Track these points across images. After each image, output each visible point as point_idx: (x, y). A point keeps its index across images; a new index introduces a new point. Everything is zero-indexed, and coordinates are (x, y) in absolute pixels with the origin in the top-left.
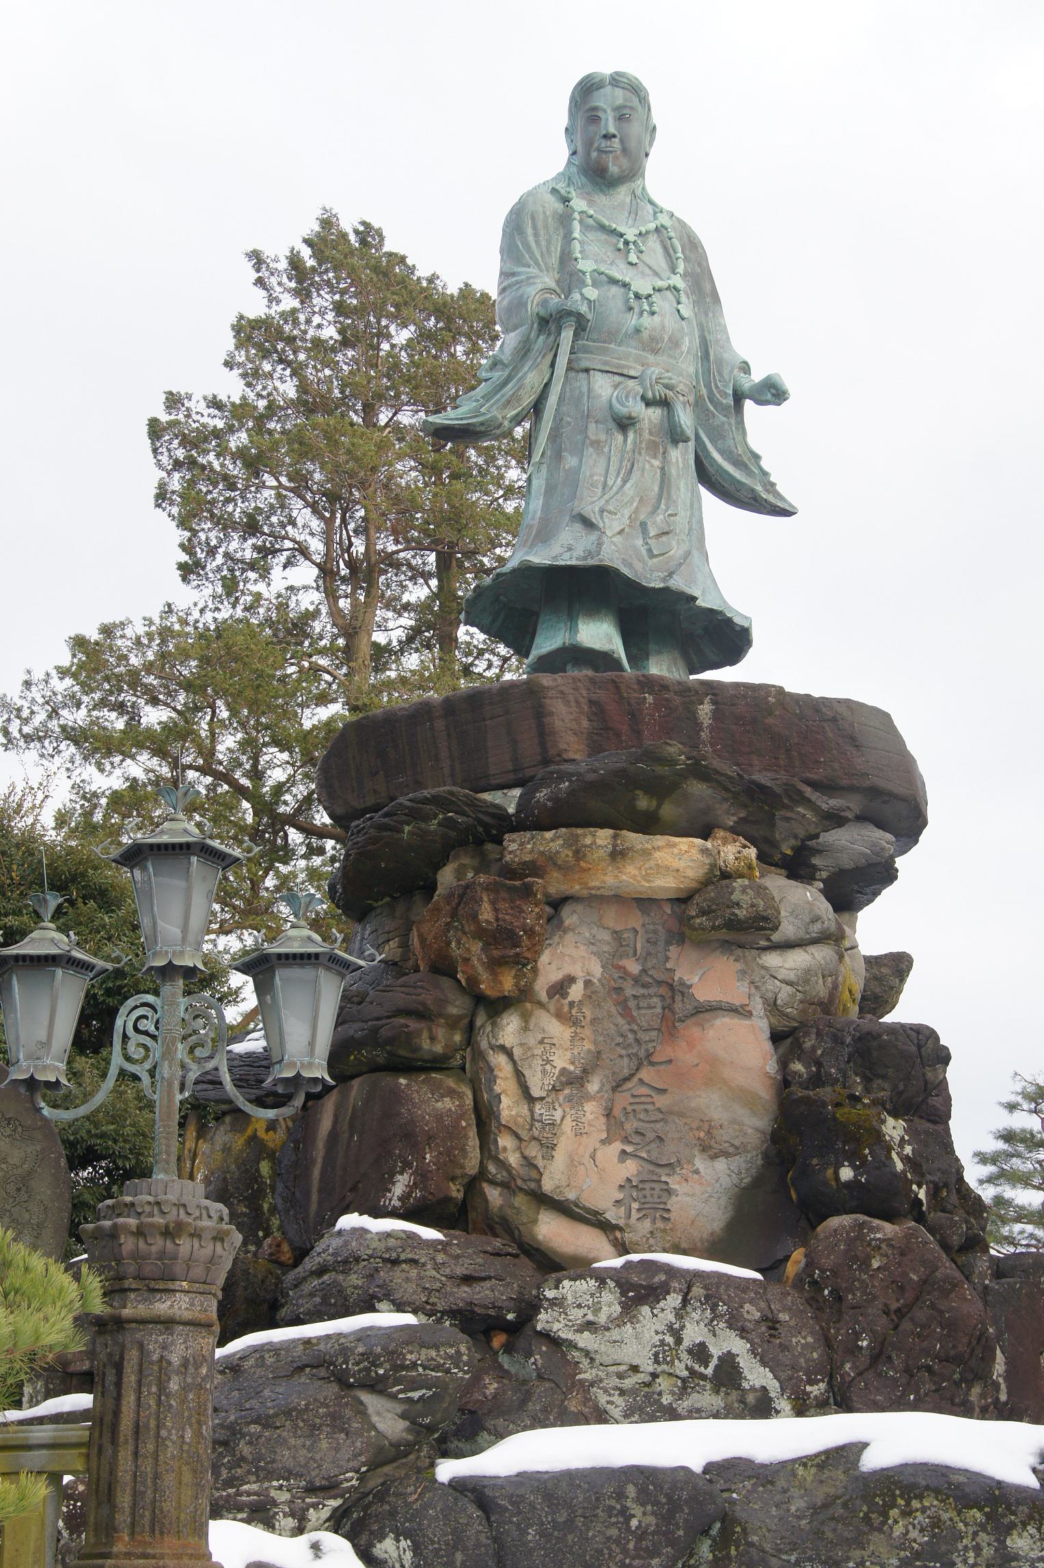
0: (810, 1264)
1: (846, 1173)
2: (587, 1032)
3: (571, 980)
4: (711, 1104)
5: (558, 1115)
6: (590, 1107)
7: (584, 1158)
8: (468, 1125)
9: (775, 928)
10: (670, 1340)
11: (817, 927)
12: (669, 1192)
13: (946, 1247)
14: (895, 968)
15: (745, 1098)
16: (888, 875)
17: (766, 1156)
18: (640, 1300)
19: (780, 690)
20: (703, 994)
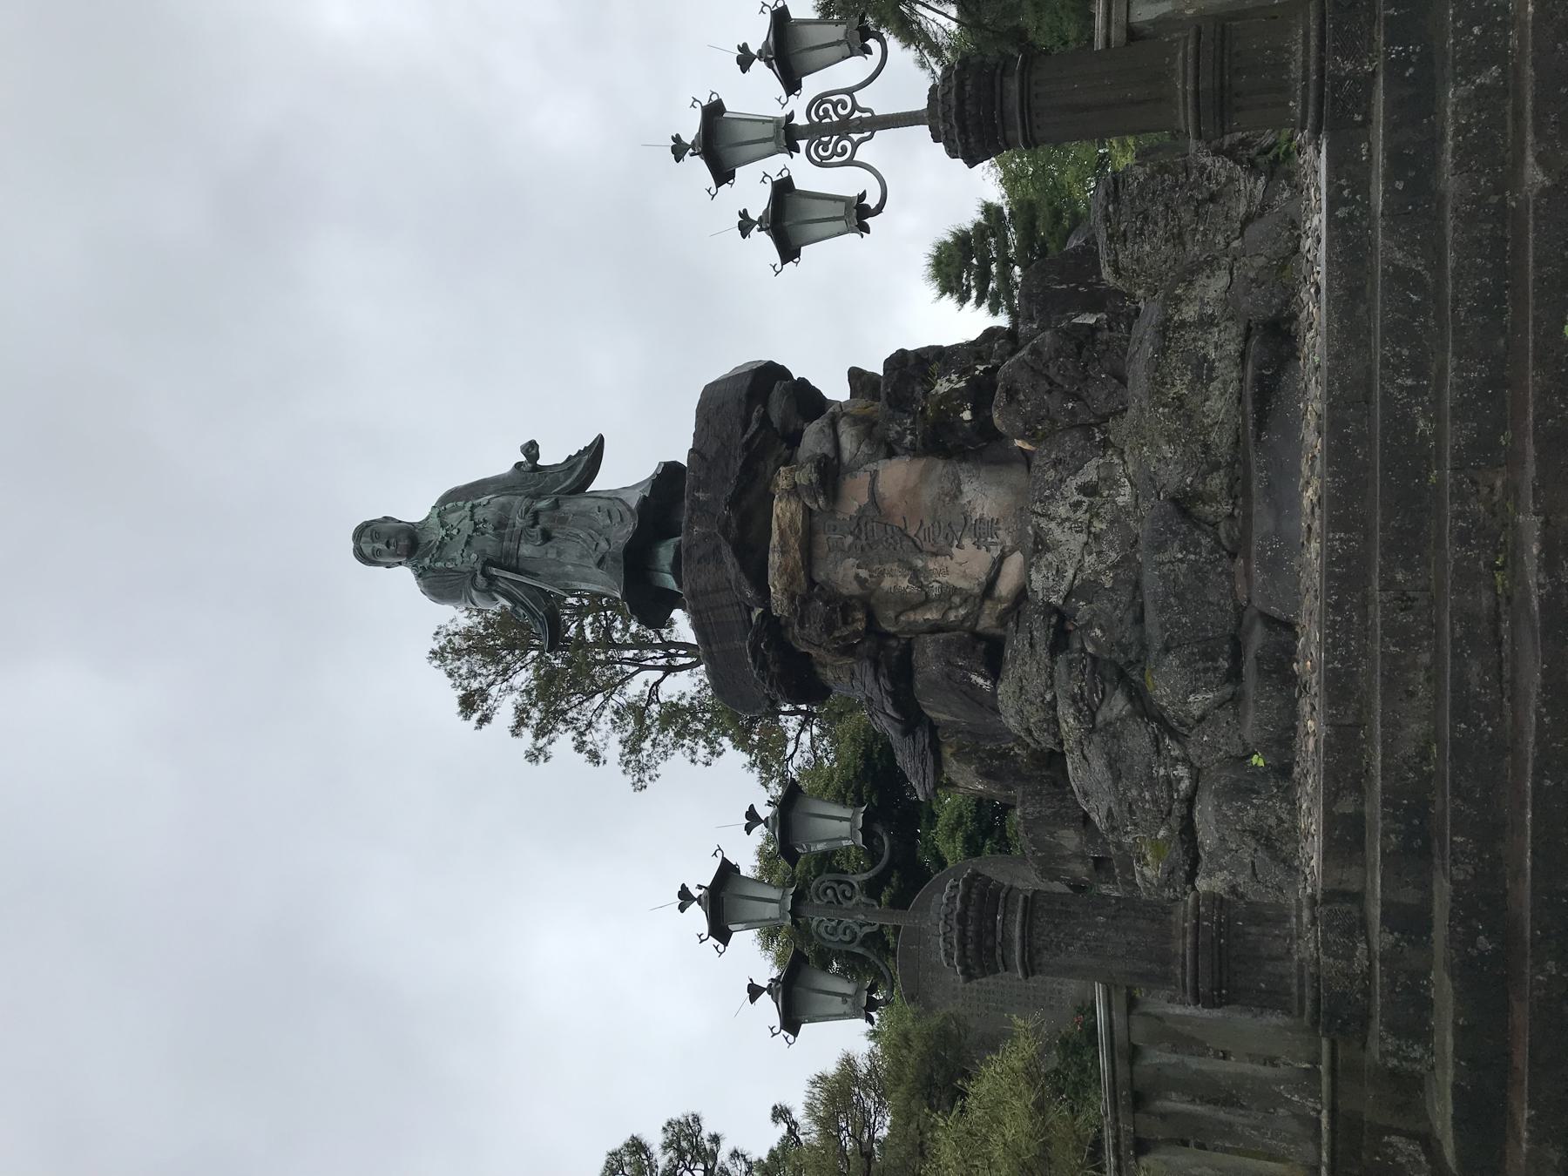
1: (967, 415)
2: (887, 566)
3: (857, 576)
4: (928, 495)
5: (936, 585)
6: (931, 566)
7: (964, 565)
8: (942, 636)
9: (825, 456)
10: (1067, 524)
11: (827, 430)
12: (981, 519)
13: (1012, 354)
14: (856, 376)
15: (924, 476)
16: (803, 382)
17: (960, 462)
18: (1043, 542)
19: (691, 451)
20: (865, 499)
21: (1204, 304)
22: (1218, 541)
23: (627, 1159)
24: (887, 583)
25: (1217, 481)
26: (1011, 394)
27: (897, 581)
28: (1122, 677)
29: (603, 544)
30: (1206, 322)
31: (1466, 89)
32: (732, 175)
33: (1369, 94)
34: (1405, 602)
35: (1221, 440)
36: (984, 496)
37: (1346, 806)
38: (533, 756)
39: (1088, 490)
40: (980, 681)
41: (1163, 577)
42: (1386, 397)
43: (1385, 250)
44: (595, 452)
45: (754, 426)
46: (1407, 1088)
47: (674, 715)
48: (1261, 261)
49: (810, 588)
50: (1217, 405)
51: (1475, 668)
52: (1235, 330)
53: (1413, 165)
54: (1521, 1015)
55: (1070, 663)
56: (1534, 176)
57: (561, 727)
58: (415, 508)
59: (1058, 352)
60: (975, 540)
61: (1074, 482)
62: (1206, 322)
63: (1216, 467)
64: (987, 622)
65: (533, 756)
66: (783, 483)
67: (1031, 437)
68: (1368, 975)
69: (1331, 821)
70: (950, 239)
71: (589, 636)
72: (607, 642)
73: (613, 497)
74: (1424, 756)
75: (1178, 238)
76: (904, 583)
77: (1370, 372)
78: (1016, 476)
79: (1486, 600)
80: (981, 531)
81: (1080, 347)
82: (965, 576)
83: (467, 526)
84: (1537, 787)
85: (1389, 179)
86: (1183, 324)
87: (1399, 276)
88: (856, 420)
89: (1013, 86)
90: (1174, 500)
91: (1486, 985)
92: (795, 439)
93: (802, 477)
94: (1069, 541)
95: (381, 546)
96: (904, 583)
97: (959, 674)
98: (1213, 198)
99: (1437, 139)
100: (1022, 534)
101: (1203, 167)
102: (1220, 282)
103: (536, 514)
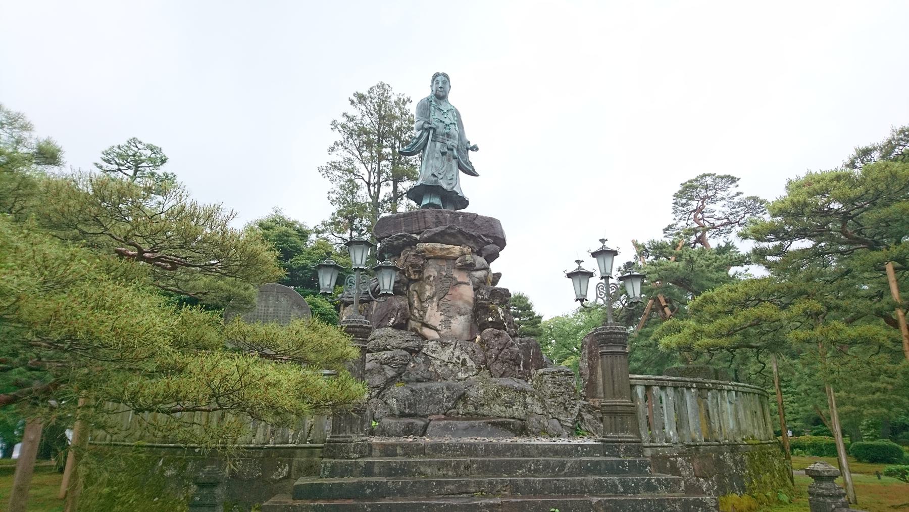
0: (482, 338)
1: (490, 319)
4: (460, 303)
7: (434, 316)
8: (408, 307)
14: (498, 276)
15: (467, 302)
16: (498, 256)
21: (532, 405)
22: (450, 409)
23: (158, 156)
24: (428, 287)
25: (471, 409)
26: (498, 335)
27: (429, 291)
28: (399, 375)
29: (440, 177)
30: (525, 406)
31: (617, 482)
32: (594, 257)
33: (614, 456)
34: (467, 467)
35: (485, 410)
36: (459, 324)
37: (399, 450)
38: (334, 123)
39: (464, 362)
40: (392, 321)
41: (438, 389)
42: (527, 462)
43: (571, 461)
44: (472, 173)
45: (486, 239)
46: (310, 470)
47: (352, 187)
48: (546, 424)
49: (426, 257)
50: (497, 409)
51: (452, 487)
52: (522, 415)
53: (594, 468)
54: (352, 502)
55: (406, 356)
56: (595, 500)
57: (346, 136)
58: (453, 98)
59: (512, 353)
60: (445, 321)
61: (467, 357)
62: (525, 406)
63: (476, 408)
64: (413, 324)
65: (334, 123)
66: (465, 249)
67: (482, 342)
68: (349, 458)
69: (394, 446)
70: (529, 302)
71: (384, 150)
72: (382, 157)
73: (457, 179)
74: (421, 473)
75: (553, 396)
76: (428, 294)
77: (533, 457)
78: (466, 336)
79: (473, 490)
80: (447, 322)
81: (514, 360)
82: (430, 316)
83: (447, 121)
84: (423, 504)
85: (590, 461)
86: (525, 398)
87: (563, 465)
88: (486, 277)
89: (620, 350)
90: (464, 394)
91: (357, 492)
92: (479, 254)
93: (468, 257)
94: (445, 355)
95: (440, 85)
96: (428, 294)
97: (395, 314)
98: (566, 408)
99: (602, 475)
100: (446, 337)
101: (575, 405)
102: (539, 411)
103: (452, 150)
